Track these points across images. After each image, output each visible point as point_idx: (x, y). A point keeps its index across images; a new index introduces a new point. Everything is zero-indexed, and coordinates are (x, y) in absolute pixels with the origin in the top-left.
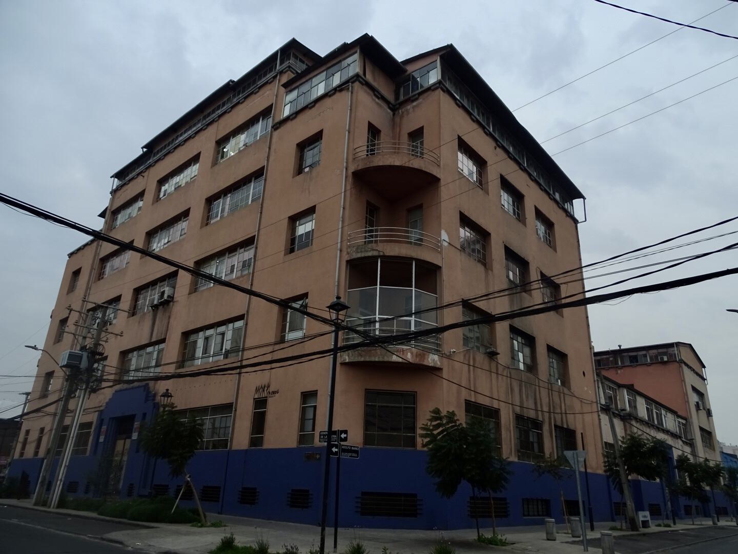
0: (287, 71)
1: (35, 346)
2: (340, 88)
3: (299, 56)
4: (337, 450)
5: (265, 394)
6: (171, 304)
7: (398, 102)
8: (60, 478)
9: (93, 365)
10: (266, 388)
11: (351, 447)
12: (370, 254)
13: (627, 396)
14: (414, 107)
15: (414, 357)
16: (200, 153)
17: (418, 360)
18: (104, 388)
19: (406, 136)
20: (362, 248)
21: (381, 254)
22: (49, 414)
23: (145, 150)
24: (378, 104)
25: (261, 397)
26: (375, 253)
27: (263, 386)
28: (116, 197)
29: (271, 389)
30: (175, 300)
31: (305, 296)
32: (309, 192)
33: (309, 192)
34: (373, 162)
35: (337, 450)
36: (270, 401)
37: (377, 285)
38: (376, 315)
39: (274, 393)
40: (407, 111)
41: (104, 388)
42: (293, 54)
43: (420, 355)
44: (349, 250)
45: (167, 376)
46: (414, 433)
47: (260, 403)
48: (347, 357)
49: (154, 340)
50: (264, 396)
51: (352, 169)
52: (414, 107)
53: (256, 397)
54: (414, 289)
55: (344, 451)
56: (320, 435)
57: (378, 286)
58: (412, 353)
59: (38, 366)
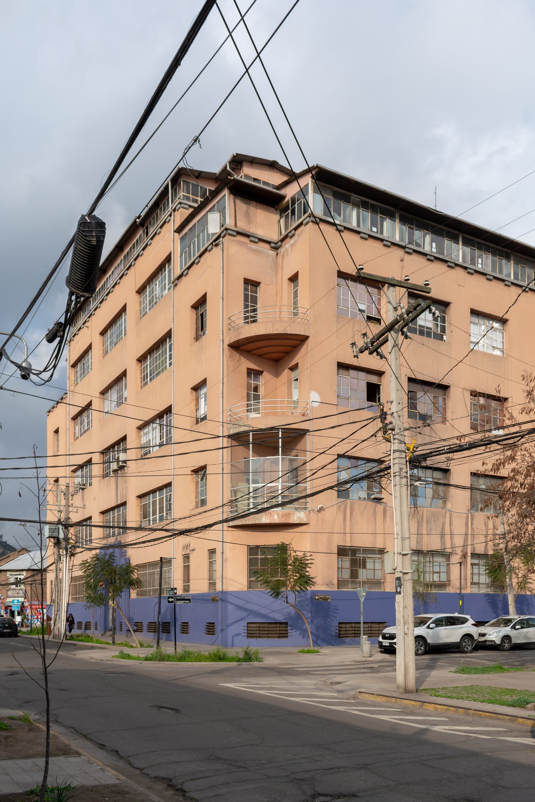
0: (179, 208)
3: (191, 182)
6: (126, 468)
9: (317, 391)
12: (243, 429)
14: (292, 246)
15: (281, 517)
16: (126, 304)
17: (283, 519)
18: (77, 553)
19: (287, 281)
21: (251, 429)
24: (255, 251)
26: (247, 429)
29: (191, 548)
39: (193, 550)
40: (286, 250)
41: (77, 553)
42: (184, 181)
43: (286, 515)
47: (186, 558)
49: (119, 503)
51: (226, 343)
52: (292, 246)
54: (280, 456)
55: (178, 600)
58: (278, 515)
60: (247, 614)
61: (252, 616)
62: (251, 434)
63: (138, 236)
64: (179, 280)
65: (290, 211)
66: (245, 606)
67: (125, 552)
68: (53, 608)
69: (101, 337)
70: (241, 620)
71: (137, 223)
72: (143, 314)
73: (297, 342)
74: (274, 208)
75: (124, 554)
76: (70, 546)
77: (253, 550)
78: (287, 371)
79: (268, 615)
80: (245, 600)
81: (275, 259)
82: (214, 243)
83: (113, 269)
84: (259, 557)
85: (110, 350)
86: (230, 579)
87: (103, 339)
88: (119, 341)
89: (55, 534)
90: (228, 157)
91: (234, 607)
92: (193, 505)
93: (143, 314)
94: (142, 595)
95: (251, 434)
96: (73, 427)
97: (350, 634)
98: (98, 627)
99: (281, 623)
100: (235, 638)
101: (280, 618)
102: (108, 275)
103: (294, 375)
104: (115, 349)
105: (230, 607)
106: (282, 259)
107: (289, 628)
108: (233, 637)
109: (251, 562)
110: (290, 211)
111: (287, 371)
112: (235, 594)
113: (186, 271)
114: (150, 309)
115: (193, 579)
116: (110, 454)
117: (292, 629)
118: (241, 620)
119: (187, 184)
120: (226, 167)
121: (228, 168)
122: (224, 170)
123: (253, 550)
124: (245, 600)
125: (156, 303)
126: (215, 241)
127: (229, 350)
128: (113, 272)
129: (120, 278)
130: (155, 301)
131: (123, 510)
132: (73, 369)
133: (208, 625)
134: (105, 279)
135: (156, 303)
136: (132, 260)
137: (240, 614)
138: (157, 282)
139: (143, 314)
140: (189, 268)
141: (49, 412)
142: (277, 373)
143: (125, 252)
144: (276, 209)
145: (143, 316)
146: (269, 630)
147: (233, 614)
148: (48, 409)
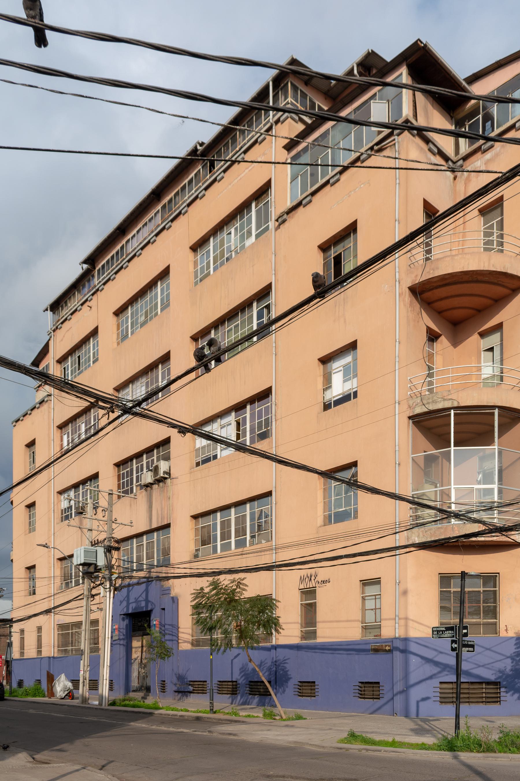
1: (46, 544)
2: (379, 146)
3: (300, 87)
4: (456, 646)
5: (313, 584)
6: (169, 481)
7: (460, 156)
8: (105, 678)
10: (313, 578)
11: (468, 641)
12: (440, 406)
13: (166, 201)
20: (429, 399)
22: (483, 666)
23: (85, 266)
25: (308, 587)
27: (309, 576)
28: (58, 341)
30: (172, 476)
31: (355, 464)
32: (345, 322)
33: (345, 322)
34: (438, 268)
35: (456, 646)
36: (320, 592)
37: (450, 447)
38: (450, 485)
42: (292, 83)
44: (411, 402)
45: (214, 572)
46: (496, 619)
48: (416, 539)
50: (311, 586)
53: (302, 587)
56: (433, 631)
57: (453, 448)
59: (12, 561)
60: (439, 669)
61: (446, 673)
62: (452, 412)
63: (192, 175)
64: (291, 214)
65: (480, 116)
66: (436, 659)
67: (169, 589)
68: (82, 662)
69: (115, 319)
70: (431, 678)
71: (198, 153)
72: (202, 277)
73: (506, 291)
74: (450, 115)
75: (167, 592)
76: (115, 576)
77: (445, 579)
78: (476, 337)
79: (471, 671)
80: (435, 650)
81: (452, 184)
82: (376, 148)
83: (140, 225)
84: (452, 590)
85: (132, 333)
86: (413, 621)
87: (117, 321)
88: (151, 319)
89: (91, 560)
90: (359, 55)
91: (419, 659)
92: (320, 521)
93: (202, 277)
94: (198, 645)
95: (452, 412)
96: (60, 438)
97: (225, 685)
98: (115, 687)
99: (488, 683)
100: (421, 704)
101: (489, 675)
102: (130, 236)
103: (494, 340)
104: (141, 332)
105: (414, 660)
106: (465, 184)
107: (503, 690)
108: (418, 702)
109: (444, 596)
110: (480, 116)
111: (476, 337)
112: (419, 641)
113: (308, 199)
114: (215, 269)
115: (320, 622)
116: (132, 465)
117: (507, 692)
118: (431, 678)
119: (295, 88)
120: (352, 69)
121: (355, 72)
122: (350, 72)
123: (445, 579)
124: (435, 650)
125: (228, 259)
126: (377, 144)
127: (409, 295)
128: (138, 232)
129: (157, 235)
130: (226, 256)
131: (157, 537)
132: (59, 365)
133: (219, 683)
134: (124, 242)
135: (228, 259)
136: (185, 204)
137: (430, 669)
138: (233, 230)
139: (199, 277)
140: (313, 194)
141: (17, 421)
142: (455, 342)
143: (166, 200)
144: (452, 118)
145: (201, 280)
146: (468, 693)
147: (418, 669)
148: (16, 417)
